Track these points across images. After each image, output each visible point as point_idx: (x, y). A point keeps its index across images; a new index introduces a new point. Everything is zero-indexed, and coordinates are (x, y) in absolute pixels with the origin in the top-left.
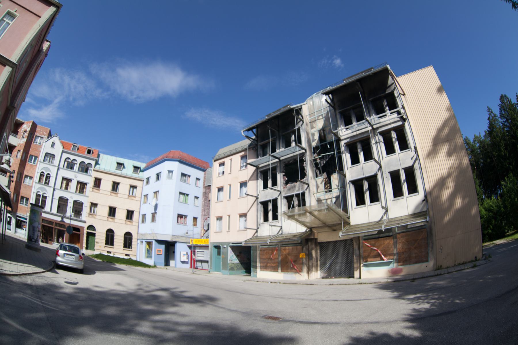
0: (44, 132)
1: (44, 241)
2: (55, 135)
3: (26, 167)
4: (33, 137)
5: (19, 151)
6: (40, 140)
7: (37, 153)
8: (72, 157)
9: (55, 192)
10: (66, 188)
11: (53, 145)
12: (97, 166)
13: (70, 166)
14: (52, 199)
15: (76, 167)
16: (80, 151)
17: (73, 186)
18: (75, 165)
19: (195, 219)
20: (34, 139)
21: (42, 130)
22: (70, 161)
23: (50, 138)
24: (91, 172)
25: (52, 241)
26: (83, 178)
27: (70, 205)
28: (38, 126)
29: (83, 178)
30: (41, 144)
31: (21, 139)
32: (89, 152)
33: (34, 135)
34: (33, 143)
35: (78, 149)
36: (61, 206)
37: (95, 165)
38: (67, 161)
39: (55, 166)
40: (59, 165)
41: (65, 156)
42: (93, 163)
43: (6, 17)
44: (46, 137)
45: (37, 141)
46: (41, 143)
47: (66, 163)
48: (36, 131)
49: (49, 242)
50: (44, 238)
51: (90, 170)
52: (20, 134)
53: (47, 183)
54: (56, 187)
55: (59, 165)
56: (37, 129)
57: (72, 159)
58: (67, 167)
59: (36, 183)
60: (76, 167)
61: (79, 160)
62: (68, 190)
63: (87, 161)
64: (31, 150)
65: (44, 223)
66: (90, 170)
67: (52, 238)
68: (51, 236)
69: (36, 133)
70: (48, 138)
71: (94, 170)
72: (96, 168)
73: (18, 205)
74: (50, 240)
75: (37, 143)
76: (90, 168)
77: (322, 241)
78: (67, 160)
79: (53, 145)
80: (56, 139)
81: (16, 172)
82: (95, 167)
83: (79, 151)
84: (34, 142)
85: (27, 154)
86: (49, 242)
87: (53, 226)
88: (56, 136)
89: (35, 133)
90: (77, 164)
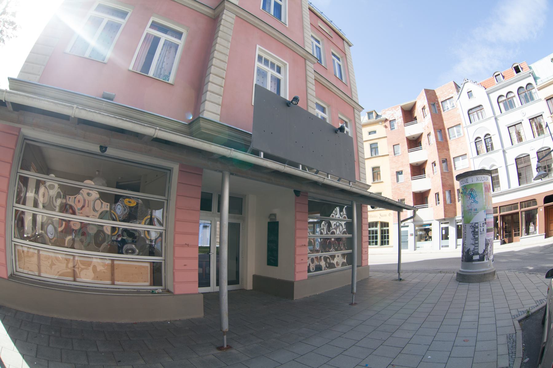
0: (450, 90)
1: (506, 240)
2: (465, 82)
3: (450, 148)
4: (439, 106)
5: (429, 135)
6: (450, 104)
7: (456, 119)
8: (504, 92)
9: (506, 154)
10: (520, 139)
11: (470, 93)
12: (538, 81)
13: (509, 105)
14: (507, 167)
15: (516, 100)
16: (507, 77)
17: (526, 130)
18: (514, 99)
19: (437, 194)
20: (441, 108)
21: (444, 91)
22: (504, 98)
23: (460, 90)
24: (537, 94)
25: (518, 235)
26: (532, 109)
27: (374, 229)
28: (435, 91)
29: (532, 109)
30: (455, 106)
31: (424, 120)
32: (517, 70)
33: (438, 103)
34: (443, 113)
35: (503, 77)
36: (522, 172)
37: (536, 82)
38: (501, 102)
39: (490, 118)
40: (494, 113)
41: (494, 96)
42: (531, 80)
43: (30, 191)
44: (455, 92)
45: (447, 107)
46: (455, 105)
47: (501, 105)
48: (438, 97)
49: (515, 238)
50: (506, 236)
51: (535, 93)
52: (419, 117)
53: (489, 148)
54: (505, 147)
55: (494, 113)
56: (437, 94)
57: (505, 95)
58: (506, 109)
59: (474, 158)
60: (516, 100)
61: (514, 88)
62: (523, 140)
63: (523, 84)
64: (445, 122)
65: (504, 211)
66: (535, 93)
67: (519, 231)
68: (517, 228)
69: (439, 100)
70: (458, 91)
71: (539, 89)
72: (538, 84)
73: (455, 204)
74: (515, 235)
75: (448, 109)
76: (533, 91)
77: (302, 279)
78: (500, 100)
79: (470, 93)
80: (469, 86)
81: (436, 163)
82: (537, 84)
83: (505, 78)
84: (444, 111)
85: (443, 131)
86: (515, 238)
87: (519, 210)
88: (467, 81)
89: (438, 101)
90: (514, 96)
